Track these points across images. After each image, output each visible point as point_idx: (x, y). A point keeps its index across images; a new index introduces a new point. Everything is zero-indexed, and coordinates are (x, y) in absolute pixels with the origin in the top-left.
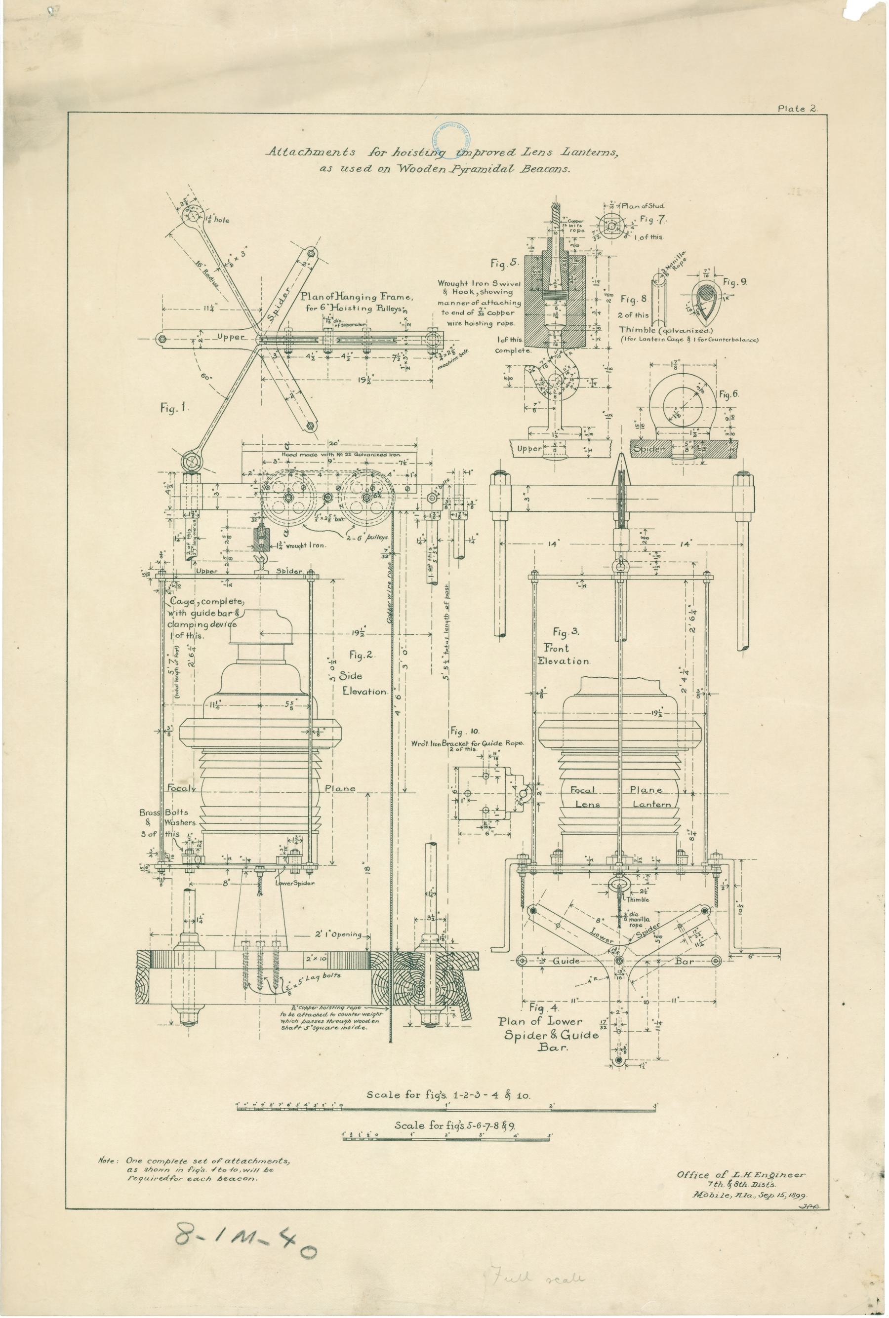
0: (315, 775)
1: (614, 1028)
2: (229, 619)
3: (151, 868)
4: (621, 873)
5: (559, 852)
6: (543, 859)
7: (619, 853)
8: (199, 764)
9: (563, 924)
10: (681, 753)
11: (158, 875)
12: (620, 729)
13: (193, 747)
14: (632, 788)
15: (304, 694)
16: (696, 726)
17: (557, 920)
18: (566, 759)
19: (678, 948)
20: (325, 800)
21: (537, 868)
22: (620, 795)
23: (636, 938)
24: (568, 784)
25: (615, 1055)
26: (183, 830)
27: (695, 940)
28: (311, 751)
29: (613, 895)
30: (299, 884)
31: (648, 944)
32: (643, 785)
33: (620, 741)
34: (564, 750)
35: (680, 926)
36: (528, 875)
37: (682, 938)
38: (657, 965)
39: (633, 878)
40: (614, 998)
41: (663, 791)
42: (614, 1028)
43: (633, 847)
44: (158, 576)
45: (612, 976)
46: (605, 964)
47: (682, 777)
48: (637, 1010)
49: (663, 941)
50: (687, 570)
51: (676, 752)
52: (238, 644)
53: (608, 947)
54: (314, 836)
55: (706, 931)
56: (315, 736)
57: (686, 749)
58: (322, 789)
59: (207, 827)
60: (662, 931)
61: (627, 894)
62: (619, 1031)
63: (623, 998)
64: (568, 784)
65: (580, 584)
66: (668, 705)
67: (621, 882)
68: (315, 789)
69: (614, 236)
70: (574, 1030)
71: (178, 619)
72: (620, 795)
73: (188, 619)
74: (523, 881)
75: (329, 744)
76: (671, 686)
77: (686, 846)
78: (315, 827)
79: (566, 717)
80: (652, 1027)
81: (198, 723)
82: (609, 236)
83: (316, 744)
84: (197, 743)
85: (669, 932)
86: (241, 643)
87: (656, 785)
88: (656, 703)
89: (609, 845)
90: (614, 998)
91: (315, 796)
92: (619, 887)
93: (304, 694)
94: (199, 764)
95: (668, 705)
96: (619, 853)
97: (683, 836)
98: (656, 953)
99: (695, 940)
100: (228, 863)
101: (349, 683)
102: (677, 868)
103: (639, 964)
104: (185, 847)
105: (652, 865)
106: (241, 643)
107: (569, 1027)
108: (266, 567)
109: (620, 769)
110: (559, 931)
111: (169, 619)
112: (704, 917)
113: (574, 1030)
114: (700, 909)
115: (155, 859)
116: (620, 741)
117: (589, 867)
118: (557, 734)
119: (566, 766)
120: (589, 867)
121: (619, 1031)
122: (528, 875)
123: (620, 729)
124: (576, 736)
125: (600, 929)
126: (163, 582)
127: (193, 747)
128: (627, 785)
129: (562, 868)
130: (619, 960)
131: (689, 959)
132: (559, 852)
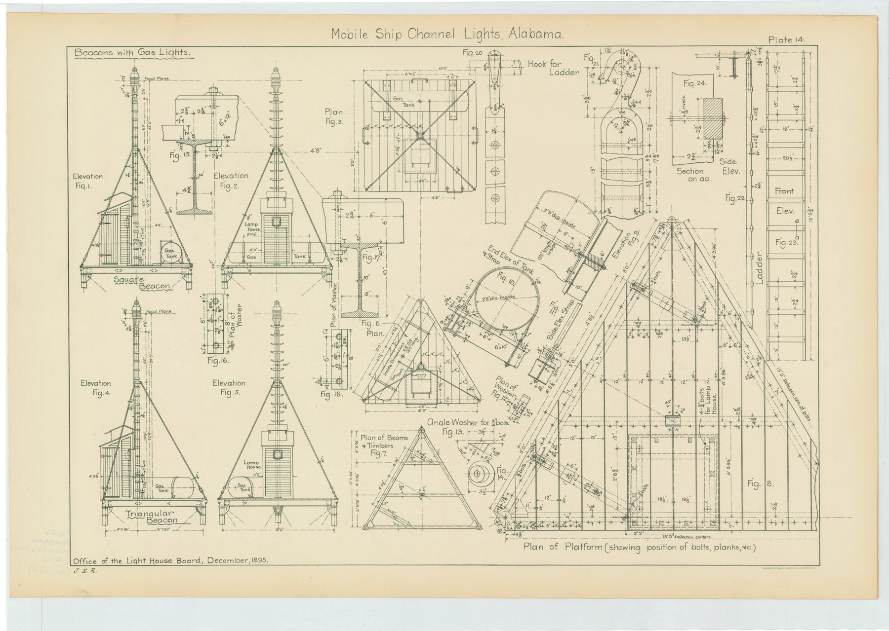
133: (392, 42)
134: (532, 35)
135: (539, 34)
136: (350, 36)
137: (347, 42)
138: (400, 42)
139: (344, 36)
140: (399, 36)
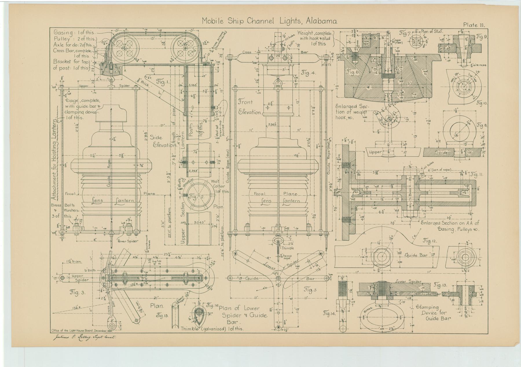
0: (139, 186)
1: (276, 311)
2: (94, 110)
3: (57, 233)
4: (279, 236)
5: (248, 225)
6: (241, 227)
7: (278, 225)
8: (81, 181)
9: (251, 260)
10: (309, 176)
11: (60, 236)
12: (278, 164)
13: (78, 173)
14: (285, 193)
15: (133, 147)
16: (316, 162)
17: (248, 258)
18: (251, 178)
19: (307, 272)
20: (144, 199)
21: (237, 232)
22: (279, 196)
23: (287, 267)
24: (253, 191)
25: (276, 325)
26: (74, 215)
27: (316, 268)
28: (137, 174)
29: (275, 246)
30: (130, 242)
31: (293, 270)
32: (289, 191)
33: (279, 169)
34: (251, 174)
35: (309, 261)
36: (233, 236)
37: (310, 267)
38: (297, 280)
39: (285, 237)
40: (276, 297)
41: (298, 194)
42: (276, 311)
43: (284, 222)
44: (60, 88)
45: (275, 285)
46: (271, 280)
47: (309, 188)
48: (287, 302)
49: (300, 269)
50: (311, 84)
51: (306, 175)
52: (100, 122)
53: (273, 271)
54: (138, 217)
55: (321, 263)
56: (139, 167)
57: (311, 173)
58: (142, 194)
59: (84, 212)
60: (299, 264)
61: (282, 245)
62: (279, 313)
63: (281, 297)
64: (253, 191)
65: (258, 92)
66: (302, 152)
67: (279, 240)
68: (139, 193)
69: (418, 47)
70: (256, 312)
71: (70, 109)
72: (279, 196)
73: (75, 109)
74: (230, 241)
75: (146, 171)
76: (303, 143)
77: (311, 221)
78: (139, 212)
79: (251, 158)
80: (295, 311)
81: (309, 171)
82: (415, 47)
83: (139, 171)
84: (80, 171)
85: (303, 264)
86: (102, 122)
87: (294, 191)
88: (296, 151)
89: (273, 221)
90: (276, 297)
91: (139, 197)
92: (278, 242)
93: (133, 147)
94: (81, 181)
95: (302, 152)
96: (278, 225)
97: (310, 216)
98: (297, 274)
99: (316, 268)
100: (95, 231)
101: (157, 141)
102: (306, 232)
103: (288, 280)
104: (74, 222)
105: (294, 231)
106: (102, 122)
107: (253, 311)
108: (113, 84)
109: (279, 184)
110: (248, 264)
111: (65, 109)
112: (320, 257)
113: (256, 312)
114: (318, 252)
115: (59, 229)
116: (279, 169)
117: (263, 231)
118: (247, 166)
119: (84, 182)
120: (263, 231)
121: (279, 313)
122: (233, 236)
123: (278, 164)
124: (256, 167)
125: (270, 264)
126: (62, 91)
127: (78, 173)
128: (282, 192)
129: (250, 232)
130: (278, 278)
131: (312, 277)
132: (248, 225)
133: (238, 25)
134: (320, 22)
135: (258, 22)
136: (213, 22)
137: (211, 25)
138: (242, 26)
139: (209, 22)
140: (242, 22)
